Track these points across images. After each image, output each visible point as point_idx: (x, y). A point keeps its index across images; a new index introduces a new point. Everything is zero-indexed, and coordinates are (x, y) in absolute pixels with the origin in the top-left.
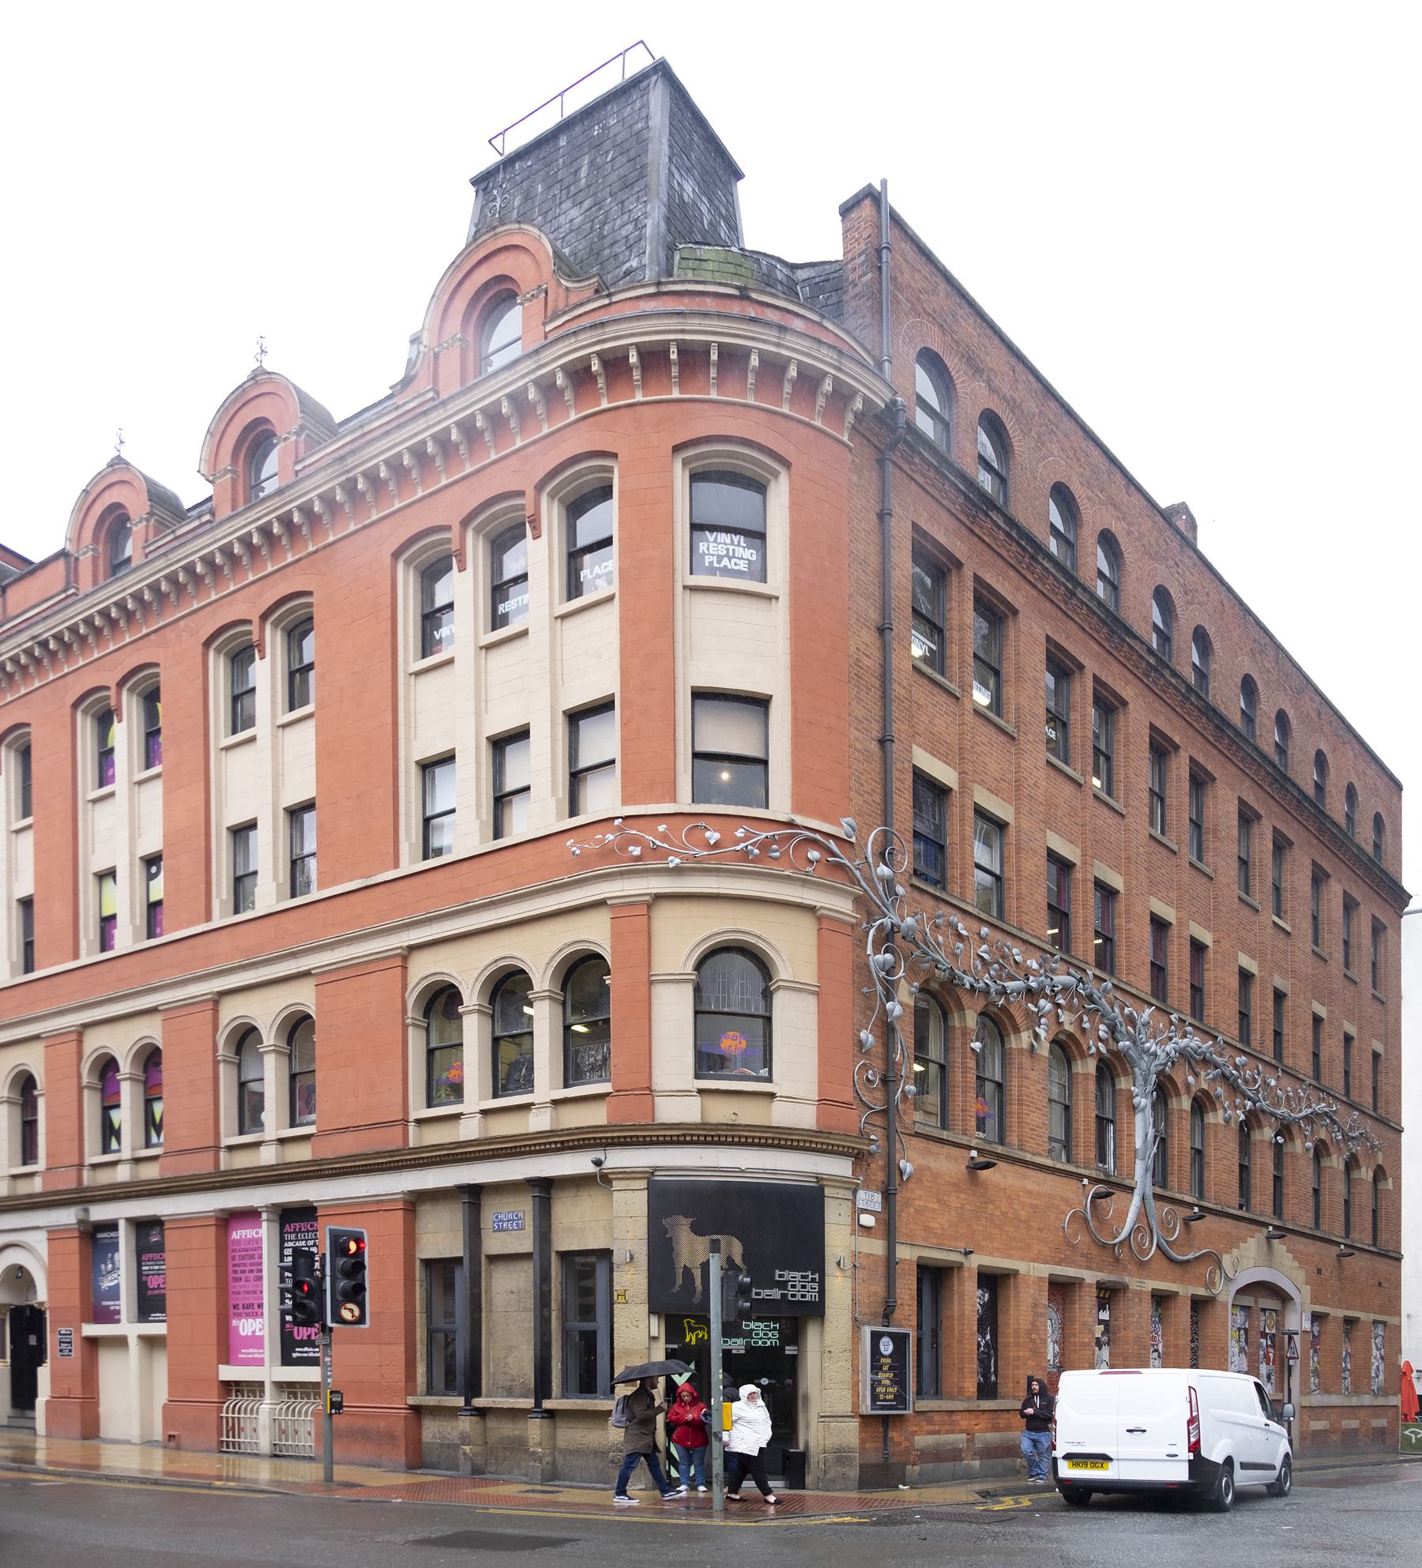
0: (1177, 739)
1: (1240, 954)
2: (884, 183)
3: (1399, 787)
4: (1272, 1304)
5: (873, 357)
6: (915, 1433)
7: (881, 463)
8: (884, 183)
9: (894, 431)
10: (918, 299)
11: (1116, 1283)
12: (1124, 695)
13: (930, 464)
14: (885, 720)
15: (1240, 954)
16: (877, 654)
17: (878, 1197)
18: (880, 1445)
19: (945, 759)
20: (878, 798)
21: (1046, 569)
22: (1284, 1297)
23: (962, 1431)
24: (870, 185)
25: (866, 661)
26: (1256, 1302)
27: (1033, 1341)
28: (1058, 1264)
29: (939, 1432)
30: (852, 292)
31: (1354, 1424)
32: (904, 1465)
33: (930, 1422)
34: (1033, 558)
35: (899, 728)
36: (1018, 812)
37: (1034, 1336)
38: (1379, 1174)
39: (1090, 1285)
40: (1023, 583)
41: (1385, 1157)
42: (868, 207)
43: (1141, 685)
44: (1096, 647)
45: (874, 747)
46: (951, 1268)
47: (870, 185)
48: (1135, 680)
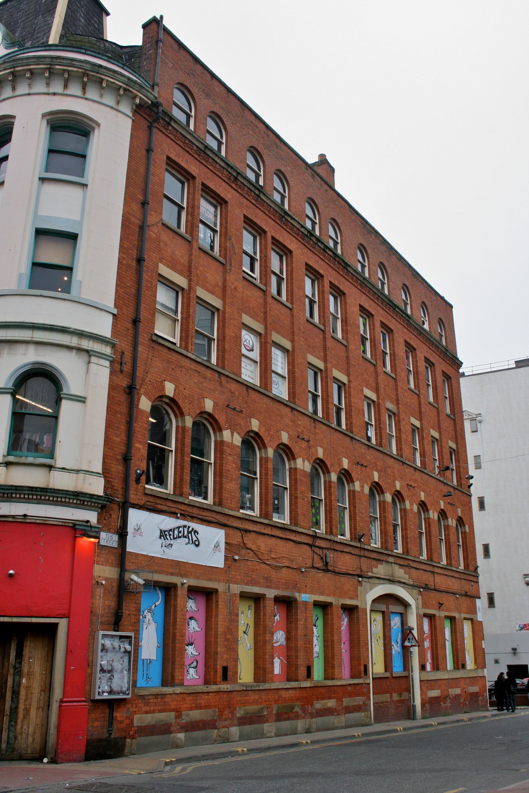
0: (322, 272)
1: (365, 389)
2: (162, 17)
3: (451, 307)
4: (400, 609)
5: (261, 199)
6: (135, 713)
7: (150, 128)
8: (162, 17)
9: (157, 113)
10: (177, 63)
11: (288, 597)
12: (290, 247)
13: (321, 248)
14: (140, 248)
15: (365, 389)
16: (139, 215)
17: (116, 537)
18: (106, 723)
19: (181, 273)
20: (133, 291)
21: (243, 183)
22: (406, 605)
23: (171, 710)
24: (155, 17)
25: (133, 219)
26: (387, 608)
27: (227, 640)
28: (247, 584)
29: (153, 712)
30: (144, 57)
31: (458, 691)
32: (125, 738)
33: (147, 704)
34: (324, 250)
35: (149, 255)
36: (224, 304)
37: (229, 636)
38: (460, 521)
39: (270, 598)
40: (231, 189)
41: (462, 511)
42: (154, 27)
43: (300, 243)
44: (273, 223)
45: (134, 264)
46: (171, 588)
47: (155, 17)
48: (296, 240)
